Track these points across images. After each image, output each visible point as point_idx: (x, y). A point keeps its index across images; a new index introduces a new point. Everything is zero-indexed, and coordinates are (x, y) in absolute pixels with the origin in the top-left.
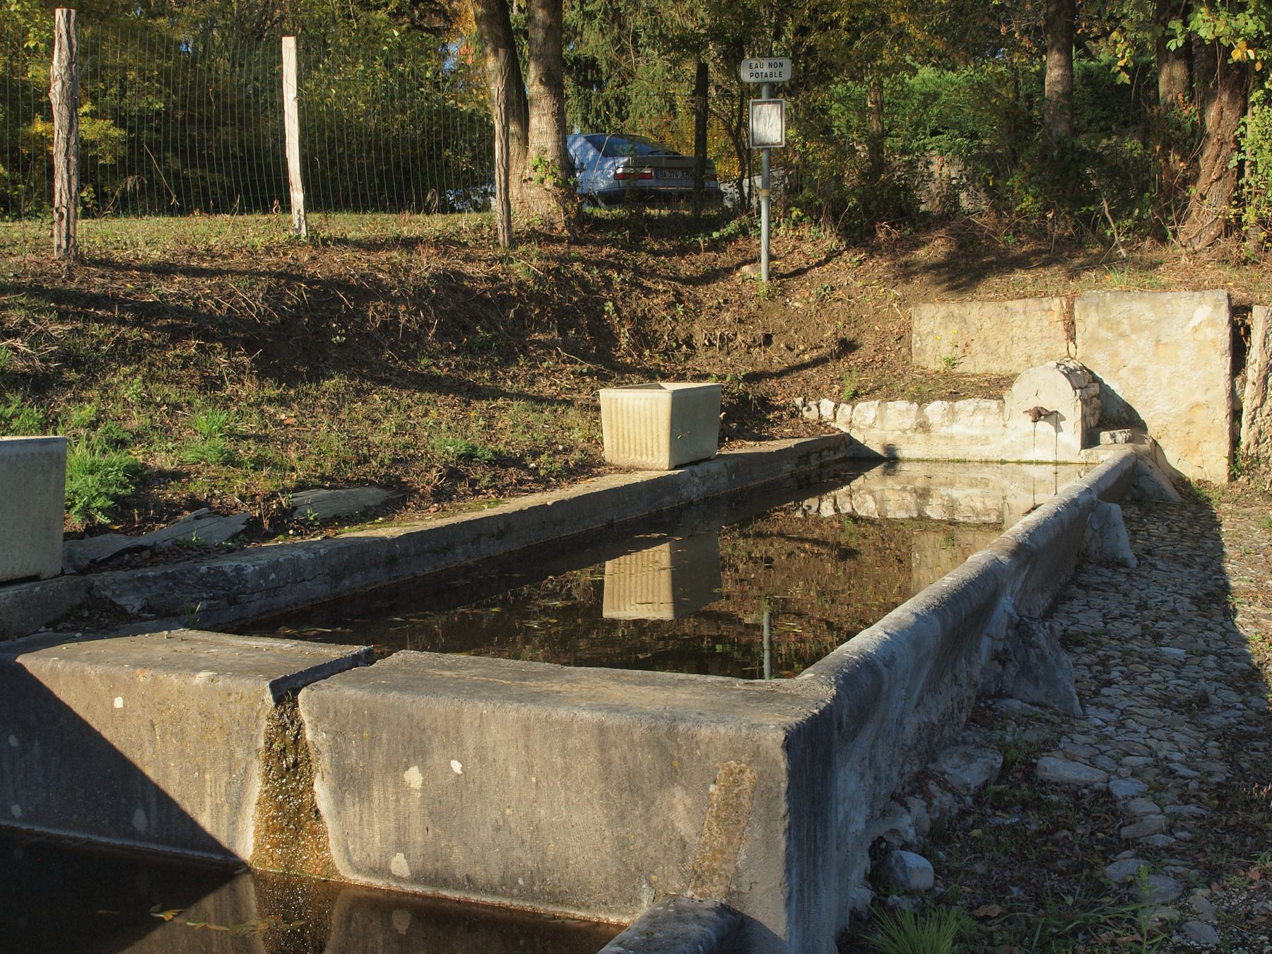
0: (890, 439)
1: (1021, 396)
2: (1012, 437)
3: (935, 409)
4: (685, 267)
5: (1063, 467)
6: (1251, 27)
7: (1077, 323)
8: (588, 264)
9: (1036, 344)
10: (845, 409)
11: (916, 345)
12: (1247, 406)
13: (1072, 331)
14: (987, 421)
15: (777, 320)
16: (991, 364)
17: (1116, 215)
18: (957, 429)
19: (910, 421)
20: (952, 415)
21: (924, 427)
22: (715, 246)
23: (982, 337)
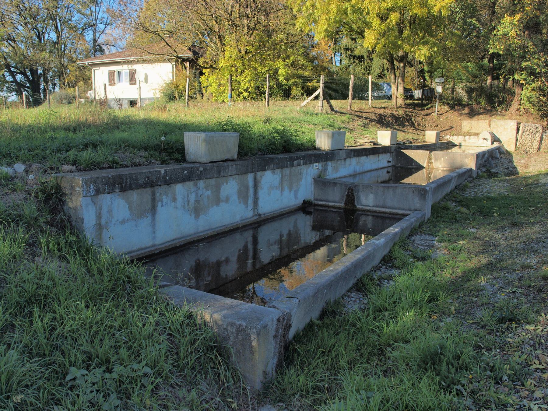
0: (460, 142)
1: (481, 136)
3: (467, 138)
4: (423, 113)
6: (524, 77)
8: (409, 112)
10: (452, 137)
11: (463, 127)
12: (519, 139)
15: (438, 122)
17: (498, 106)
18: (470, 141)
19: (462, 139)
20: (470, 139)
21: (465, 140)
22: (427, 109)
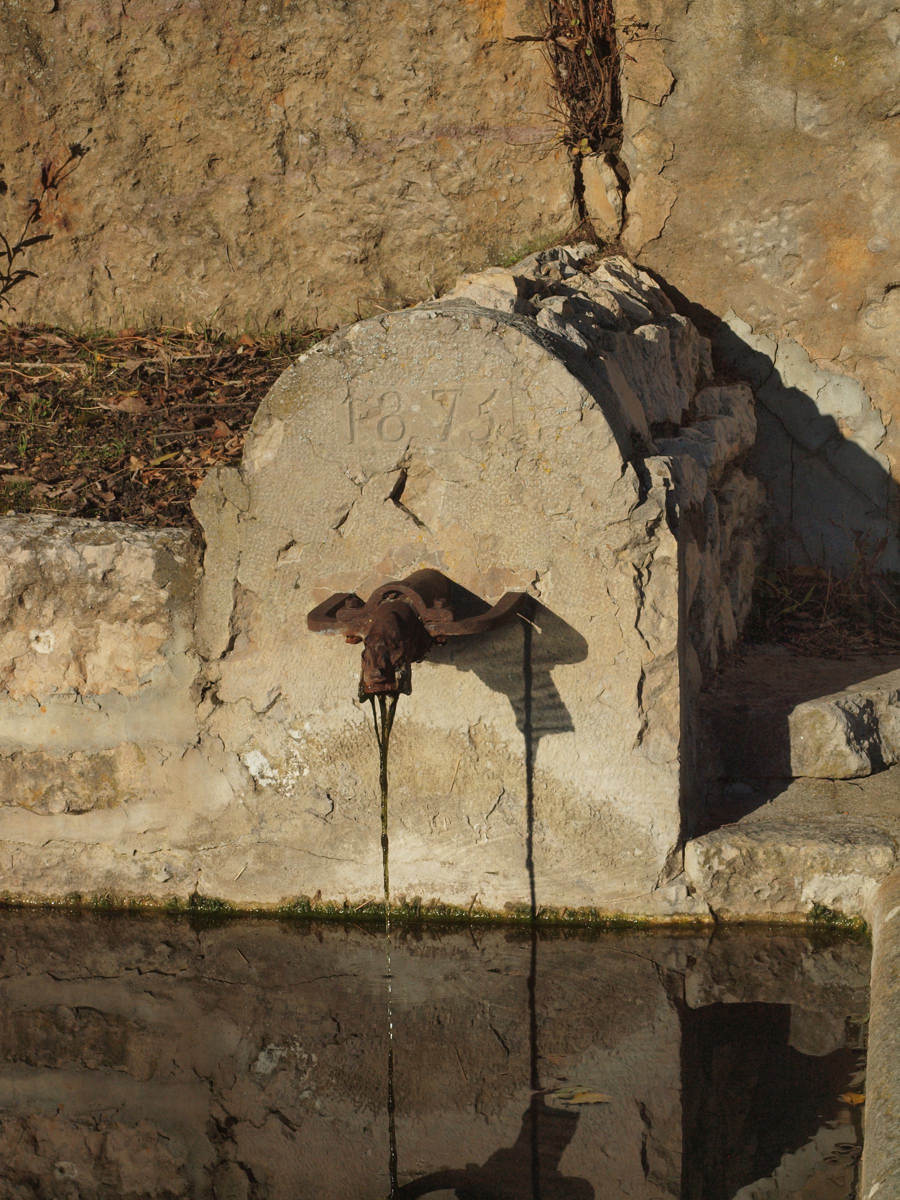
2: (255, 762)
5: (574, 947)
7: (626, 46)
9: (406, 168)
13: (601, 96)
14: (96, 664)
16: (175, 282)
23: (128, 135)
